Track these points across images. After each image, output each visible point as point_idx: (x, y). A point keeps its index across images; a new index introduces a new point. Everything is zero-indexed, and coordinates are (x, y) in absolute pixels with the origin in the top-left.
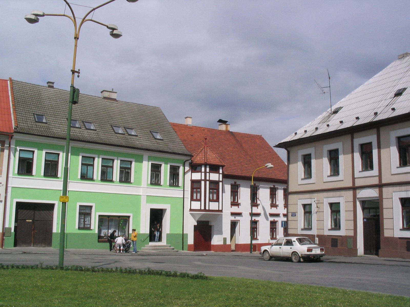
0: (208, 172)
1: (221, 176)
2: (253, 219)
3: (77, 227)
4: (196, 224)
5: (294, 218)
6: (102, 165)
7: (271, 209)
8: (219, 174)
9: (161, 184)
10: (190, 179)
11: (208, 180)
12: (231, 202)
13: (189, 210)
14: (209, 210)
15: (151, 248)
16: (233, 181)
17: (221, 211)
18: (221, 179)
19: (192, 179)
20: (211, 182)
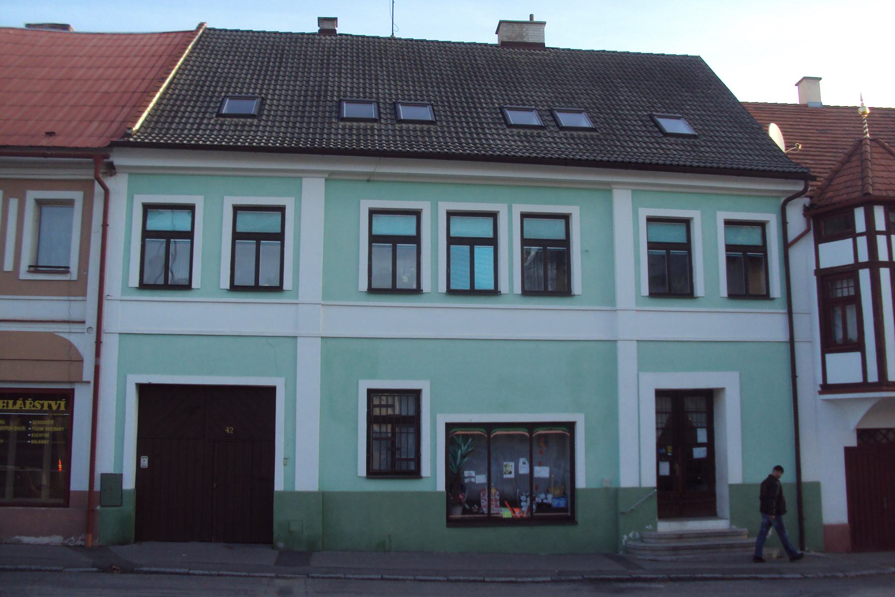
0: (881, 233)
3: (362, 471)
6: (649, 243)
9: (772, 296)
10: (814, 268)
11: (884, 264)
13: (820, 389)
15: (663, 544)
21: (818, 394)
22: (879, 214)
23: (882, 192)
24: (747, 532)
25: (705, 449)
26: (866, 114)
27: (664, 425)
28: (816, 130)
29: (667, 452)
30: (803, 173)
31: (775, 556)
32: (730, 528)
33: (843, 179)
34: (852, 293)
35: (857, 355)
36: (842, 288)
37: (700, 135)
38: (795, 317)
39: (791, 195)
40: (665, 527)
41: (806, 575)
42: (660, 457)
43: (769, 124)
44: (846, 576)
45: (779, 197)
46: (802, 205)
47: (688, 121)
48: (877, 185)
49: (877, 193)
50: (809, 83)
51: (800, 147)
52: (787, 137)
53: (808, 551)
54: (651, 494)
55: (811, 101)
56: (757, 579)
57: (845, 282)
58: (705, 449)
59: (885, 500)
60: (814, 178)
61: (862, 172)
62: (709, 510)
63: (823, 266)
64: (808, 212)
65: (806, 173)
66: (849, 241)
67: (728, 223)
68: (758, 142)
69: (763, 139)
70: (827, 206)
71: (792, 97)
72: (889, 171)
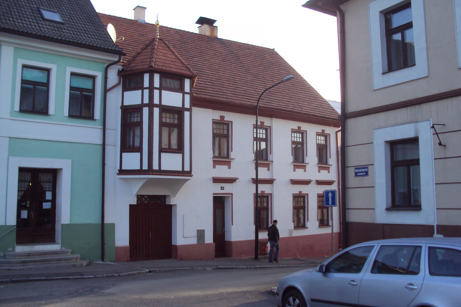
0: (156, 88)
1: (187, 97)
2: (259, 192)
4: (135, 203)
5: (365, 181)
7: (294, 171)
8: (184, 93)
10: (121, 105)
11: (156, 106)
12: (214, 157)
13: (118, 172)
14: (160, 172)
15: (18, 259)
16: (216, 115)
17: (189, 173)
18: (187, 105)
19: (125, 104)
20: (165, 109)
21: (117, 175)
22: (157, 77)
23: (159, 66)
24: (71, 251)
25: (50, 203)
26: (159, 25)
27: (25, 189)
28: (139, 34)
29: (26, 205)
30: (119, 51)
31: (84, 265)
32: (61, 249)
33: (142, 58)
34: (139, 120)
35: (138, 154)
36: (134, 117)
37: (65, 23)
38: (107, 131)
39: (111, 63)
40: (20, 249)
41: (96, 276)
42: (20, 207)
43: (108, 24)
44: (120, 275)
45: (105, 63)
46: (118, 69)
47: (61, 15)
48: (157, 62)
49: (156, 67)
50: (140, 9)
51: (123, 39)
52: (118, 34)
53: (106, 262)
54: (12, 229)
55: (140, 19)
56: (67, 279)
57: (136, 113)
58: (50, 203)
59: (150, 233)
60: (124, 55)
61: (151, 55)
62: (51, 239)
63: (125, 104)
64: (120, 73)
65: (120, 51)
66: (140, 91)
67: (73, 74)
68: (99, 32)
69: (103, 31)
70: (130, 71)
71: (130, 15)
72: (165, 56)
